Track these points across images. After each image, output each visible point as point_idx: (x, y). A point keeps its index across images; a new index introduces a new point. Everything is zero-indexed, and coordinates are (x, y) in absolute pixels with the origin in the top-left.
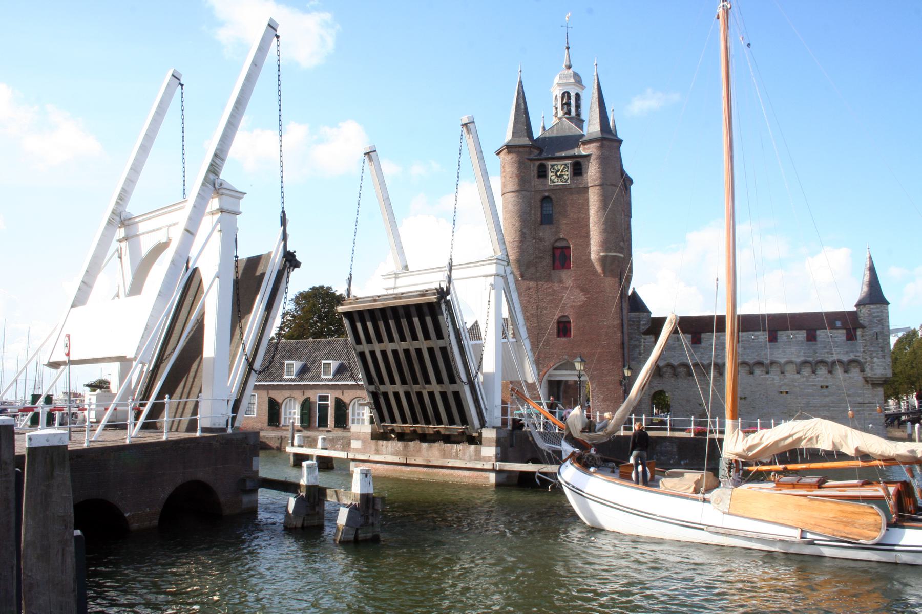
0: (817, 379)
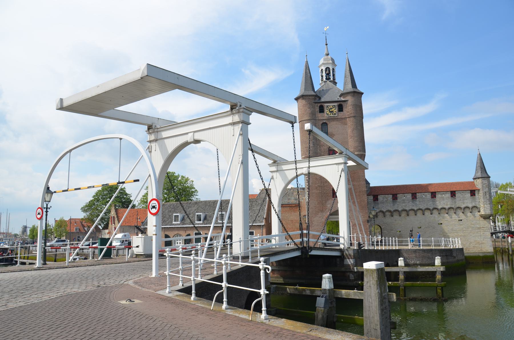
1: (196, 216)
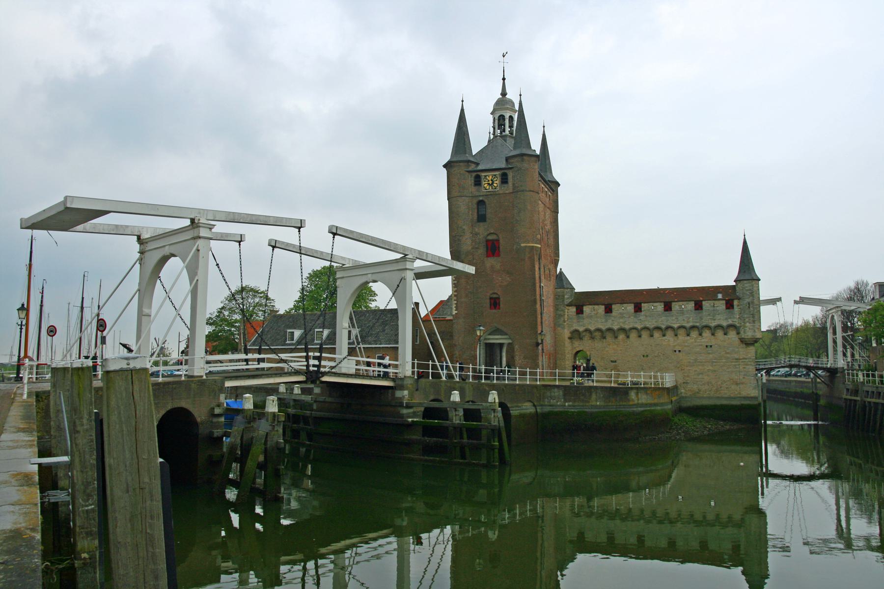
0: (703, 340)
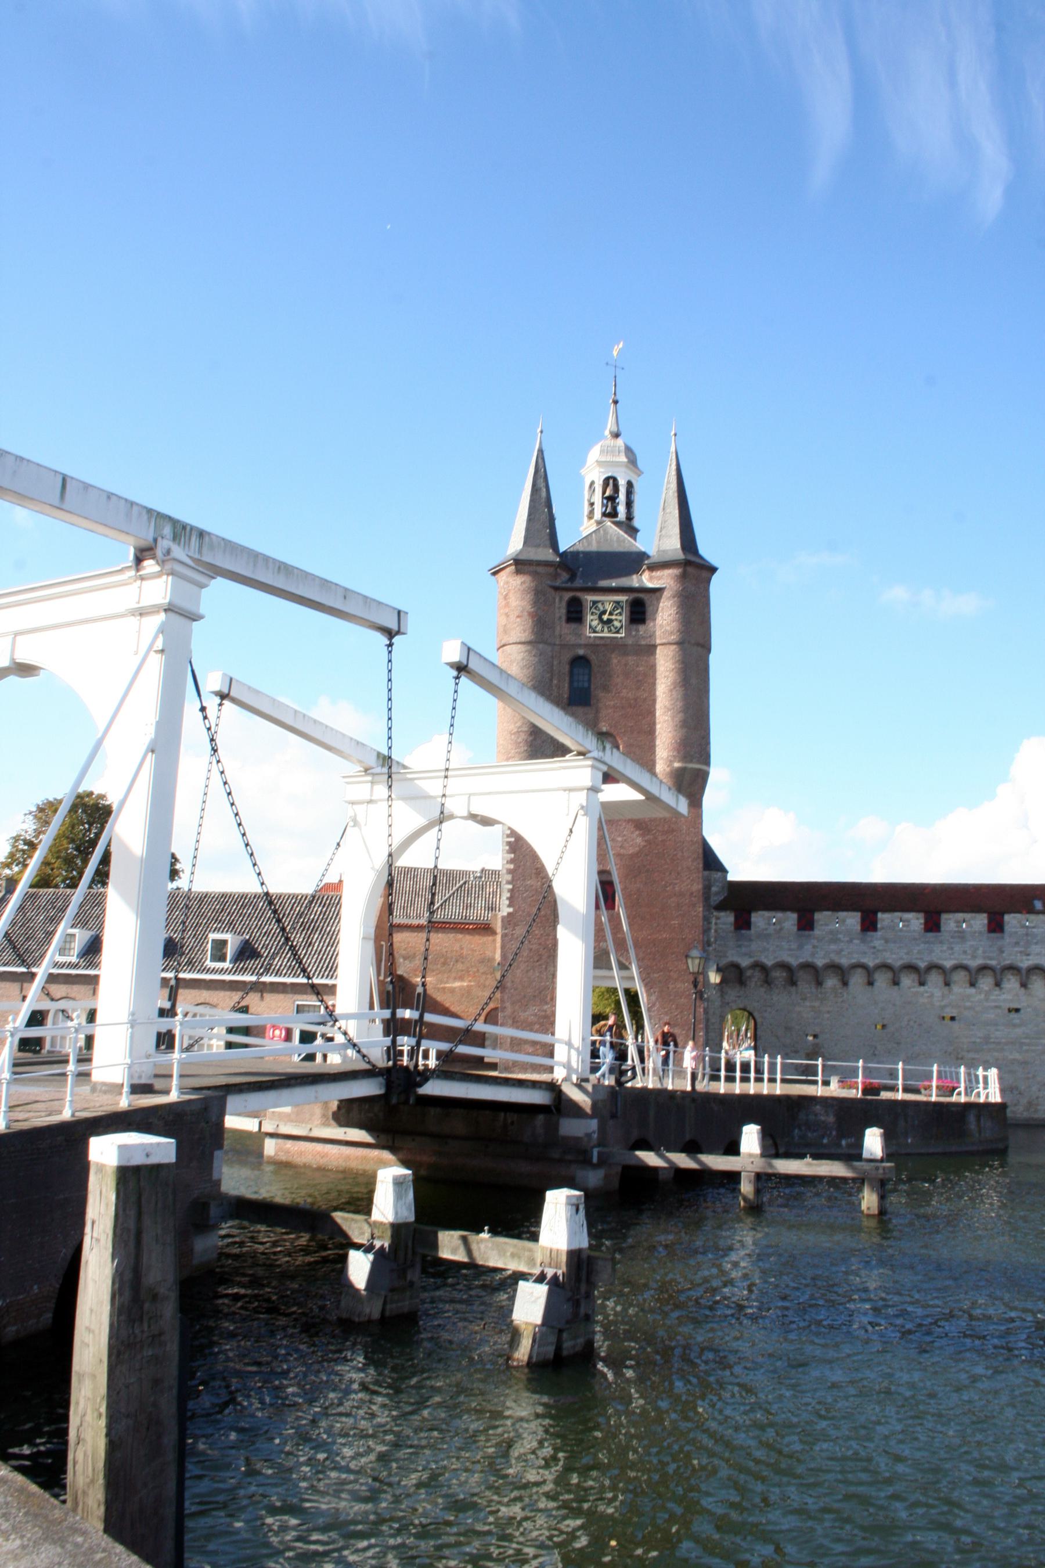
0: (1004, 997)
1: (209, 946)
